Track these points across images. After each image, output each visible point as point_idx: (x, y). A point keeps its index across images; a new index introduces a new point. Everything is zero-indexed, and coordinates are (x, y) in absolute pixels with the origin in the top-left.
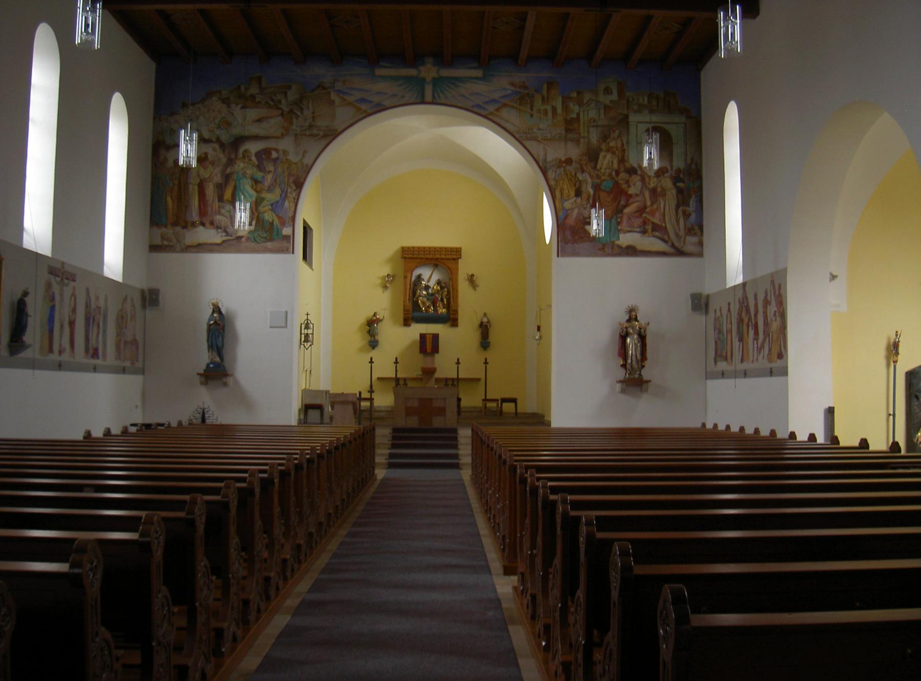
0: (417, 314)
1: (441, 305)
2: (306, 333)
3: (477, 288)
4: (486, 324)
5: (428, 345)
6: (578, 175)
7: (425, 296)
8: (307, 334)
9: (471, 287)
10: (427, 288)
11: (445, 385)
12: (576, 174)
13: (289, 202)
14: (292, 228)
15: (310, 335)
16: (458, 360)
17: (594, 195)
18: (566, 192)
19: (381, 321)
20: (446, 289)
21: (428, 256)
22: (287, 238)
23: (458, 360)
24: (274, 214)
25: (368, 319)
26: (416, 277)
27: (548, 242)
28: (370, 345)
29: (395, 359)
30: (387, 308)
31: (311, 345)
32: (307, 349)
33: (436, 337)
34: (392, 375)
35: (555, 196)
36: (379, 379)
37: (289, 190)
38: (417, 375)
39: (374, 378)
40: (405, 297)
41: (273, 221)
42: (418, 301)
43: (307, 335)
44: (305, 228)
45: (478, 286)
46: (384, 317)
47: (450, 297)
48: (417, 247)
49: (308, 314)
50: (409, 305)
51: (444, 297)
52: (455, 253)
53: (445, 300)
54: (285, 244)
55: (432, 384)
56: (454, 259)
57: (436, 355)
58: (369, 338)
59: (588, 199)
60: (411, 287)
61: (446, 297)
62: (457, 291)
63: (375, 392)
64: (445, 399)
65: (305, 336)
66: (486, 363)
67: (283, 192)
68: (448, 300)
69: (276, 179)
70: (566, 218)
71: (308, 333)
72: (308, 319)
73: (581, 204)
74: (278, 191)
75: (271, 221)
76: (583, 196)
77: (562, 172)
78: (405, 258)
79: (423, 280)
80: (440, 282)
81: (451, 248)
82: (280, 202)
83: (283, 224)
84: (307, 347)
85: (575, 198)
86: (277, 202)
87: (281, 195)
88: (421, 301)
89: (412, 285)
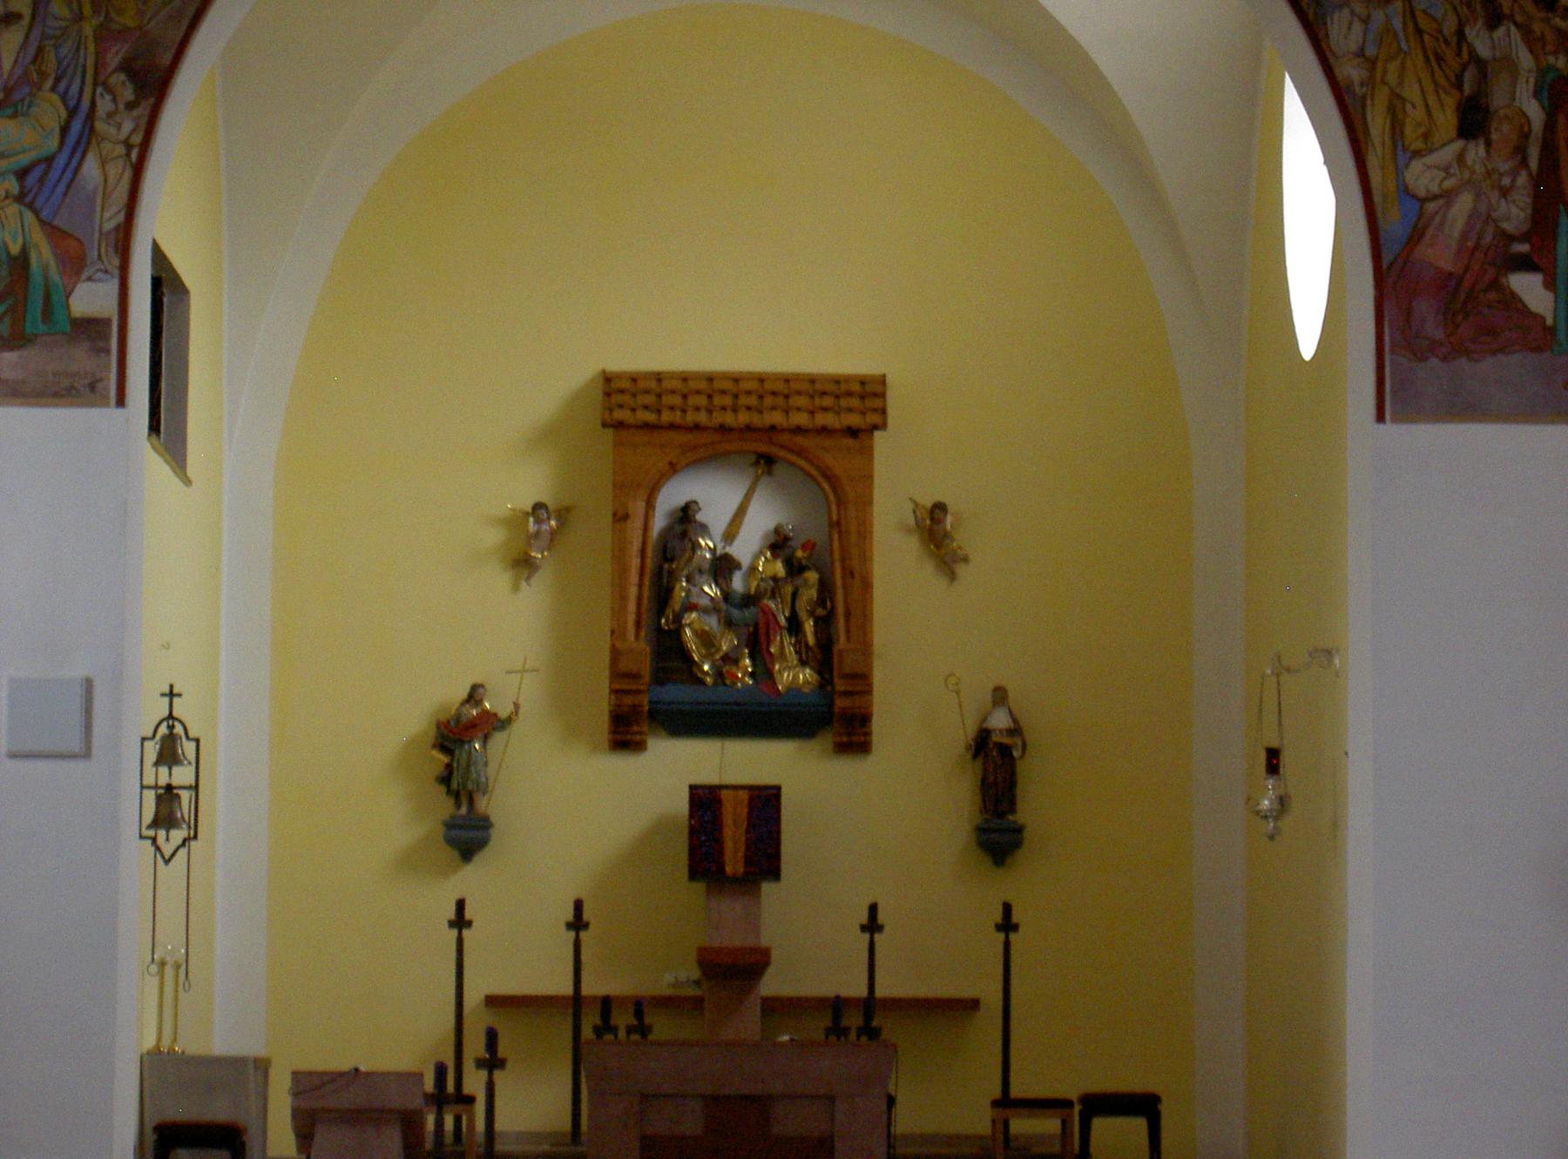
0: (676, 693)
1: (790, 650)
2: (163, 781)
3: (961, 569)
4: (1006, 740)
5: (729, 846)
6: (1470, 33)
7: (714, 608)
8: (169, 788)
9: (929, 568)
10: (723, 567)
11: (828, 1031)
12: (1460, 34)
13: (103, 163)
14: (113, 286)
15: (185, 796)
16: (873, 909)
17: (1550, 126)
18: (1416, 114)
19: (504, 724)
20: (812, 576)
21: (729, 419)
22: (91, 330)
23: (873, 909)
24: (29, 217)
25: (443, 717)
26: (672, 514)
27: (1308, 344)
28: (450, 841)
29: (453, 908)
30: (529, 665)
31: (185, 841)
32: (167, 862)
33: (765, 802)
34: (565, 987)
35: (1367, 132)
36: (493, 1001)
37: (104, 105)
38: (676, 985)
39: (473, 997)
40: (618, 611)
41: (24, 251)
42: (677, 633)
43: (168, 795)
44: (157, 283)
45: (965, 560)
46: (517, 706)
47: (832, 613)
48: (673, 375)
49: (171, 694)
50: (640, 650)
51: (803, 615)
52: (854, 402)
53: (809, 626)
54: (79, 358)
55: (748, 1024)
56: (853, 432)
57: (767, 887)
58: (444, 807)
59: (1520, 151)
60: (649, 562)
61: (811, 613)
62: (867, 586)
63: (509, 1066)
64: (831, 1099)
65: (159, 798)
66: (1007, 925)
67: (72, 113)
68: (825, 623)
69: (40, 50)
70: (1416, 235)
71: (175, 782)
72: (171, 716)
73: (1489, 173)
74: (50, 111)
75: (15, 249)
76: (1494, 136)
77: (1397, 23)
78: (619, 425)
79: (704, 529)
80: (786, 539)
81: (837, 380)
82: (61, 161)
83: (75, 264)
84: (168, 850)
85: (1459, 144)
86: (49, 160)
87: (65, 130)
88: (695, 632)
89: (650, 552)
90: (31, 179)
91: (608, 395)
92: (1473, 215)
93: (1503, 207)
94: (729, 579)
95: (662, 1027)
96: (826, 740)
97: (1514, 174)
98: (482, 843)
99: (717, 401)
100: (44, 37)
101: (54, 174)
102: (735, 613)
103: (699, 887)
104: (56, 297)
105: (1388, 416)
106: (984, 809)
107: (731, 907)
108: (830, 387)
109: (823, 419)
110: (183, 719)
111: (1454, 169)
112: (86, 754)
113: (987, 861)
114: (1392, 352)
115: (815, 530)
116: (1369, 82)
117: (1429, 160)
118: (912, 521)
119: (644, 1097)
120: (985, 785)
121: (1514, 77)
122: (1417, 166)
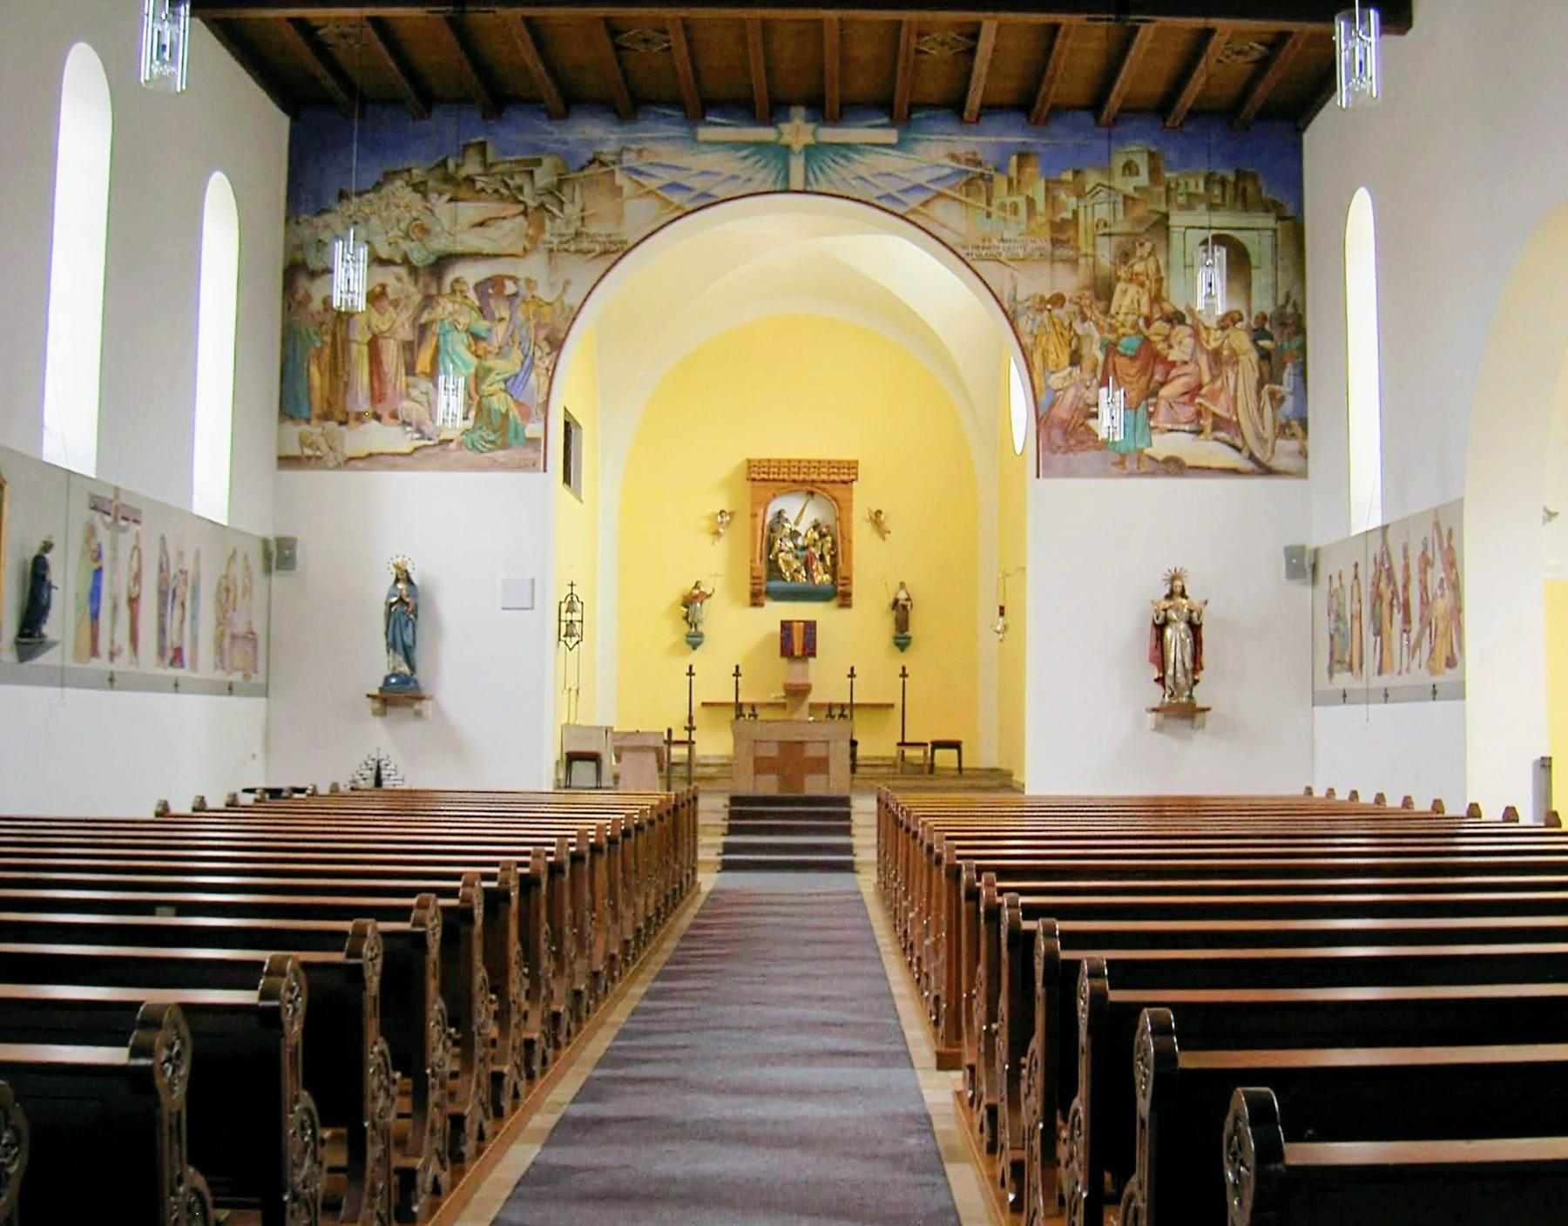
1: (820, 568)
2: (569, 619)
4: (905, 603)
8: (571, 621)
9: (875, 535)
10: (794, 535)
12: (1071, 324)
13: (538, 375)
15: (578, 624)
16: (852, 669)
20: (829, 538)
21: (796, 477)
22: (533, 441)
23: (852, 669)
24: (509, 398)
26: (774, 515)
28: (689, 642)
33: (810, 627)
35: (1033, 364)
37: (538, 354)
38: (777, 698)
39: (696, 703)
49: (572, 585)
50: (761, 568)
51: (825, 554)
53: (828, 558)
54: (530, 453)
55: (803, 713)
56: (844, 482)
57: (811, 660)
58: (686, 628)
59: (1094, 371)
61: (829, 553)
62: (850, 542)
64: (827, 742)
67: (526, 356)
69: (513, 332)
70: (1052, 406)
74: (517, 355)
75: (503, 411)
76: (1083, 366)
77: (1046, 321)
82: (521, 376)
83: (526, 416)
85: (1069, 369)
86: (516, 376)
87: (523, 363)
90: (509, 383)
91: (749, 467)
92: (1075, 396)
93: (1087, 393)
94: (797, 538)
95: (763, 714)
96: (834, 603)
97: (1091, 380)
98: (700, 643)
99: (793, 470)
100: (515, 326)
101: (519, 380)
102: (799, 553)
103: (785, 660)
104: (520, 429)
105: (1041, 475)
106: (897, 630)
107: (798, 667)
108: (836, 465)
109: (833, 477)
110: (143, 552)
111: (1068, 378)
112: (532, 608)
113: (897, 649)
114: (1043, 451)
115: (831, 521)
116: (1035, 344)
117: (1058, 375)
118: (868, 516)
119: (755, 741)
120: (897, 620)
121: (1092, 342)
122: (1053, 377)
